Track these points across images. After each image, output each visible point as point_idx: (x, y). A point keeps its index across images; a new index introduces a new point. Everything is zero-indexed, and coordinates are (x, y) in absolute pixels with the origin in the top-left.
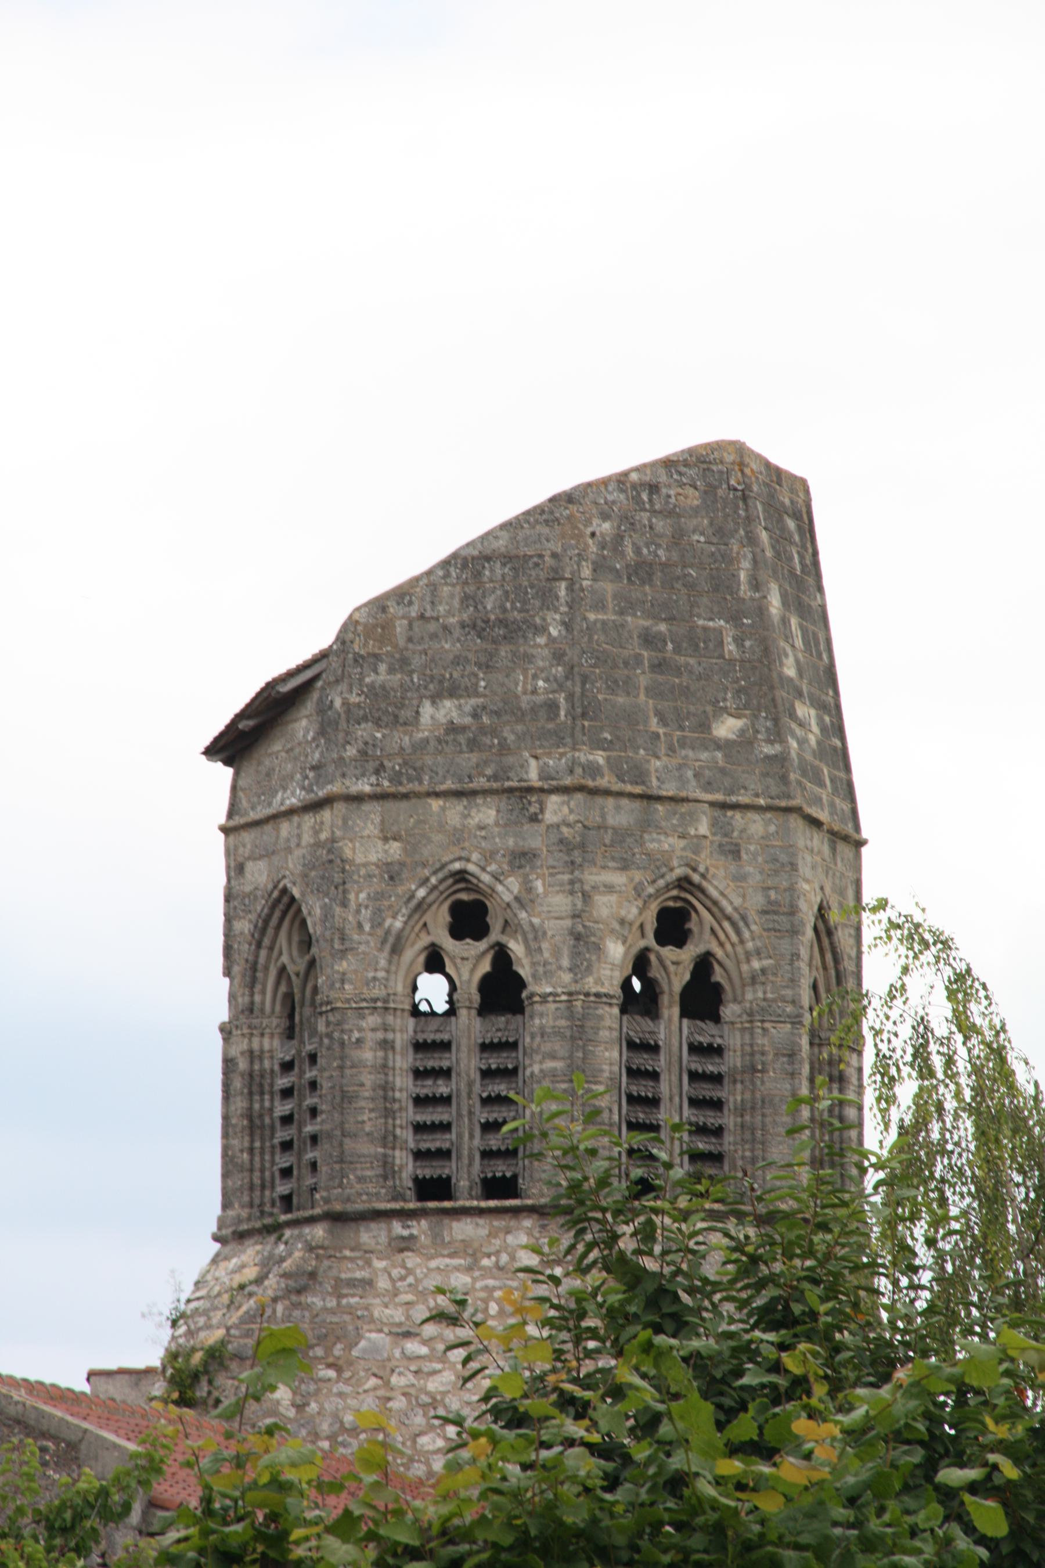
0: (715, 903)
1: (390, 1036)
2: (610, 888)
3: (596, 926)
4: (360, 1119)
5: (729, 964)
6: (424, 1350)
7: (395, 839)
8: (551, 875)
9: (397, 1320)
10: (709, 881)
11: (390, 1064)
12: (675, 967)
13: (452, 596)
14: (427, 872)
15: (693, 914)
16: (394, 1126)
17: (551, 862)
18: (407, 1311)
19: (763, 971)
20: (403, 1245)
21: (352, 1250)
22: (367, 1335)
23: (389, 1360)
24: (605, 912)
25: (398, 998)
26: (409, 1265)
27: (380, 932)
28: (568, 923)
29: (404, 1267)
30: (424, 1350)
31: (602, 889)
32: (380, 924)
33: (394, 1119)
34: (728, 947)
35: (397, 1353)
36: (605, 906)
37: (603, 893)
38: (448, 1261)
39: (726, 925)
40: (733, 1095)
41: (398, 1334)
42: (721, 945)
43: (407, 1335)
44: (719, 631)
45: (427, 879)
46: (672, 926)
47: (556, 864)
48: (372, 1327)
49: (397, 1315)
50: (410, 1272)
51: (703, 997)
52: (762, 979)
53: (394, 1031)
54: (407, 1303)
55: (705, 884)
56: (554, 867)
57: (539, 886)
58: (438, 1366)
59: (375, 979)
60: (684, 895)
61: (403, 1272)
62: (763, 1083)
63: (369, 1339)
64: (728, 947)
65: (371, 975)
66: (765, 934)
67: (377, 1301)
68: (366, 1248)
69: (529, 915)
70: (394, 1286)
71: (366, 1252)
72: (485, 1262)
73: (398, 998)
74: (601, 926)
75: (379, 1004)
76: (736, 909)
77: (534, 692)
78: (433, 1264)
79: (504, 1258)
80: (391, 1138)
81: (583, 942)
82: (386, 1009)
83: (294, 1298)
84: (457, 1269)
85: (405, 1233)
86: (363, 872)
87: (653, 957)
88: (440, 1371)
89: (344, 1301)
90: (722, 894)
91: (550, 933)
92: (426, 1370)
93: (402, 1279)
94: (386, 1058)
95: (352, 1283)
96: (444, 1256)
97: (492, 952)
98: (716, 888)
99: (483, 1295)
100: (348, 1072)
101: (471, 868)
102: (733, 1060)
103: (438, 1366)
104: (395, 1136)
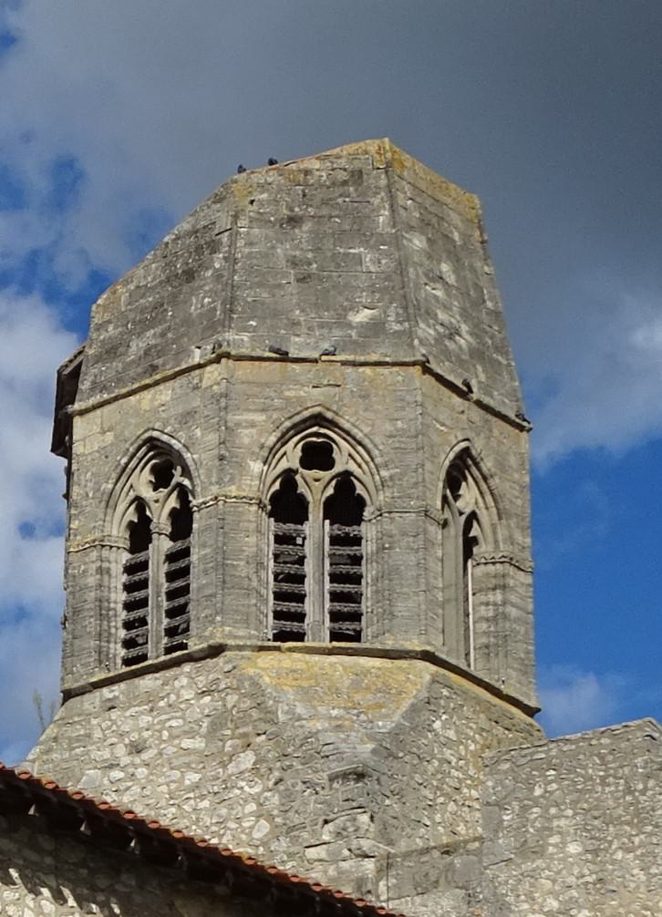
0: (348, 433)
1: (105, 565)
2: (252, 425)
3: (239, 450)
4: (84, 625)
5: (367, 479)
6: (122, 775)
7: (109, 431)
8: (206, 422)
9: (105, 757)
10: (341, 416)
11: (106, 584)
12: (316, 488)
13: (157, 269)
14: (127, 446)
15: (334, 446)
16: (109, 627)
17: (206, 413)
18: (112, 749)
19: (391, 478)
20: (109, 705)
21: (79, 715)
22: (87, 772)
23: (100, 786)
24: (246, 441)
25: (113, 539)
26: (113, 718)
27: (98, 495)
28: (215, 452)
29: (111, 720)
30: (122, 775)
31: (244, 424)
32: (99, 490)
33: (109, 622)
34: (364, 465)
35: (106, 781)
36: (246, 437)
37: (246, 427)
38: (137, 709)
39: (360, 448)
40: (368, 571)
41: (106, 767)
42: (360, 466)
43: (111, 767)
44: (360, 255)
45: (128, 450)
46: (318, 456)
47: (209, 413)
48: (91, 766)
49: (106, 754)
50: (114, 722)
51: (346, 506)
52: (390, 484)
53: (109, 562)
54: (112, 744)
55: (337, 419)
56: (208, 416)
57: (198, 432)
58: (130, 784)
59: (94, 527)
60: (323, 431)
61: (109, 723)
62: (390, 557)
63: (88, 775)
64: (364, 465)
65: (93, 525)
66: (393, 451)
67: (94, 747)
68: (87, 712)
69: (192, 454)
70: (104, 734)
71: (87, 715)
72: (162, 704)
73: (113, 539)
74: (242, 450)
75: (97, 543)
76: (366, 435)
77: (202, 306)
78: (128, 714)
79: (173, 697)
80: (106, 634)
81: (226, 459)
82: (103, 546)
83: (45, 757)
84: (142, 713)
85: (111, 696)
86: (89, 459)
87: (298, 477)
88: (130, 787)
89: (73, 752)
90: (353, 425)
91: (204, 462)
92: (122, 788)
93: (109, 728)
94: (101, 580)
95: (78, 739)
96: (135, 706)
97: (176, 492)
98: (348, 421)
99: (158, 727)
100: (77, 595)
101: (155, 434)
102: (367, 548)
103: (130, 784)
104: (110, 634)
